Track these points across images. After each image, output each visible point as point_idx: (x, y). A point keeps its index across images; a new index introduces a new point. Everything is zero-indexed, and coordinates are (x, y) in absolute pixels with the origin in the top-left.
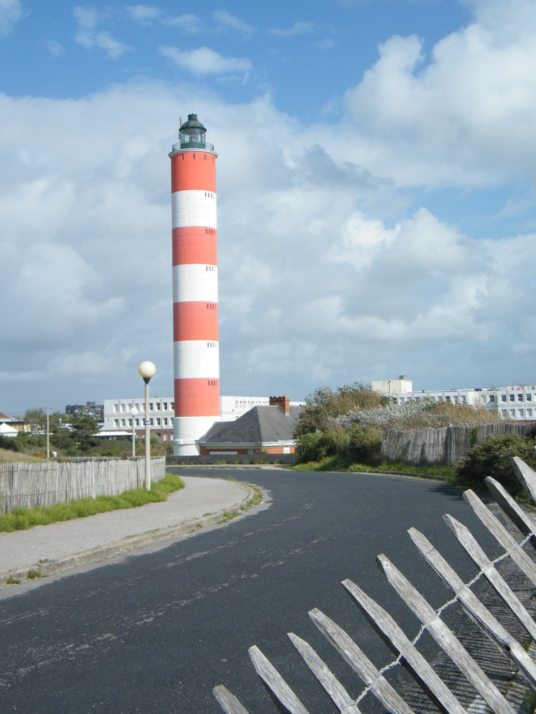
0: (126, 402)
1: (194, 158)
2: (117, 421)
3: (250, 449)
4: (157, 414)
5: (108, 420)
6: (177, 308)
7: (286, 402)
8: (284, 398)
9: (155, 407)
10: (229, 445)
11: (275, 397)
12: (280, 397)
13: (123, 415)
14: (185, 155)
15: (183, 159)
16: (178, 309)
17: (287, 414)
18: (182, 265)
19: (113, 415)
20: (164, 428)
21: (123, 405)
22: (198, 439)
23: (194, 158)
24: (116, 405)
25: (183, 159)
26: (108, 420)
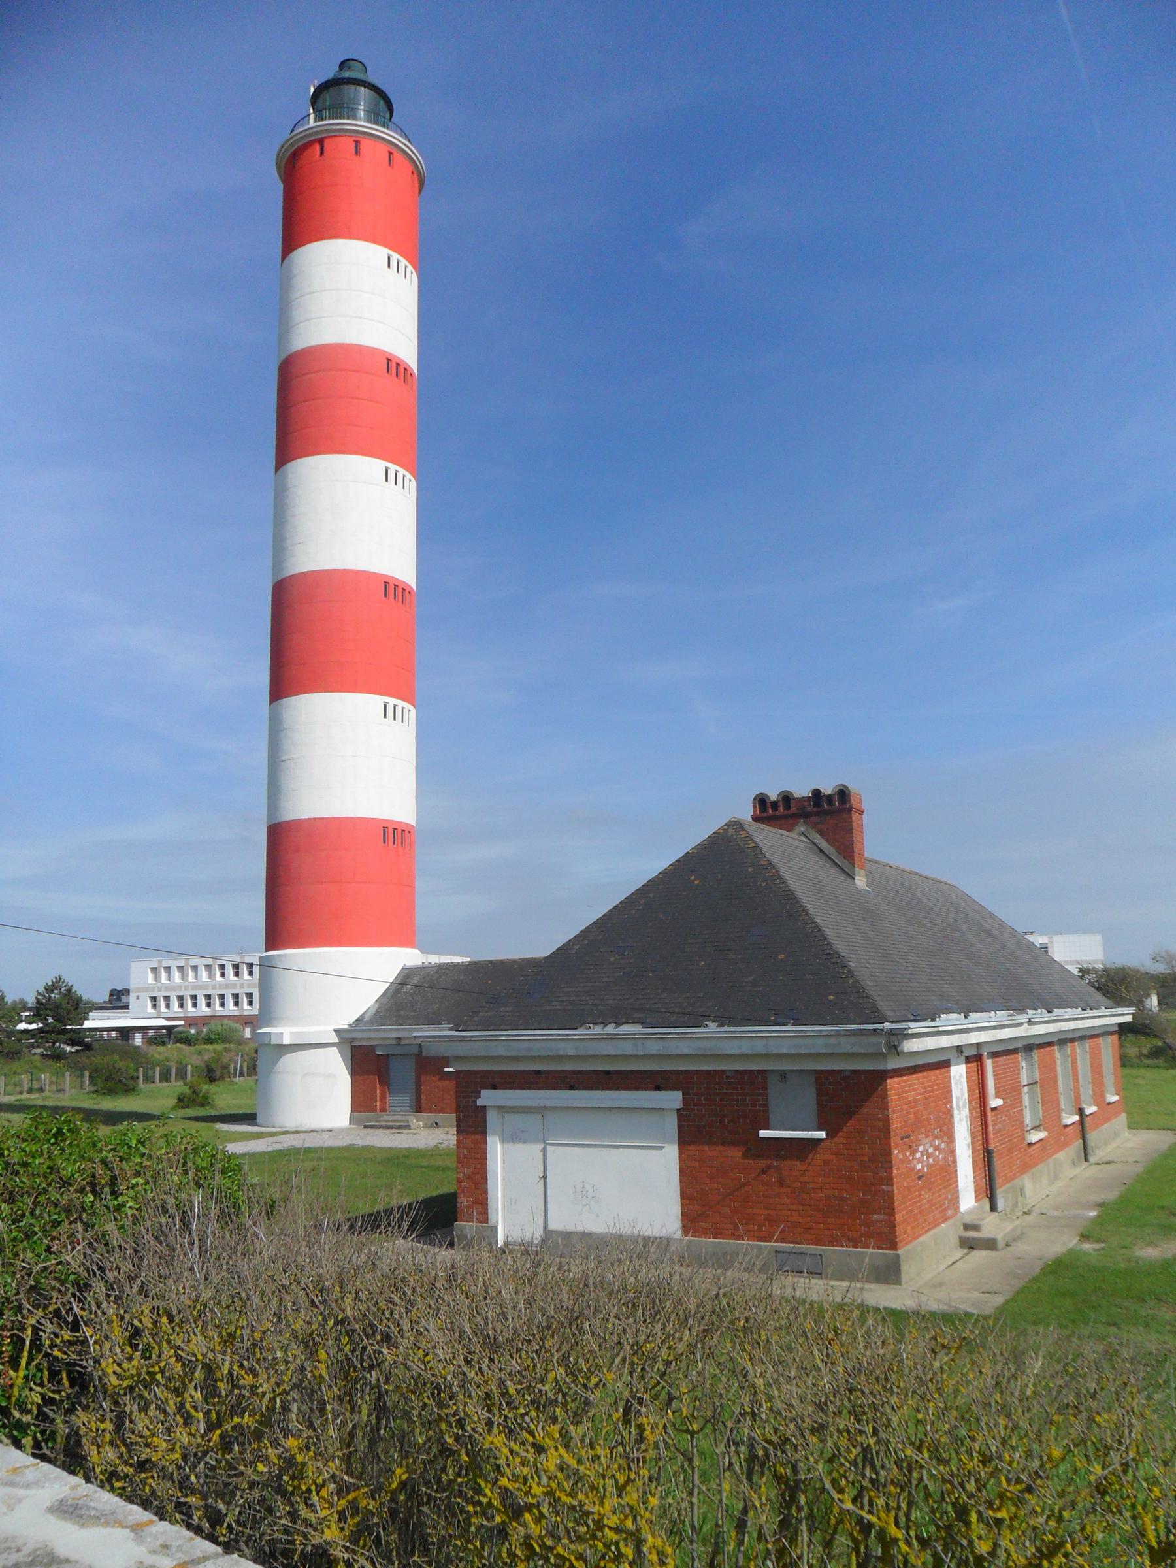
0: (174, 963)
1: (357, 152)
2: (154, 999)
3: (783, 1075)
4: (234, 986)
5: (138, 998)
6: (279, 837)
7: (855, 816)
8: (843, 793)
9: (230, 971)
10: (627, 1048)
11: (786, 798)
12: (817, 793)
13: (167, 989)
14: (326, 142)
15: (322, 153)
16: (283, 841)
17: (860, 881)
18: (299, 461)
19: (146, 990)
20: (246, 1013)
21: (168, 969)
22: (343, 1025)
23: (357, 152)
24: (154, 970)
25: (322, 153)
26: (138, 998)
